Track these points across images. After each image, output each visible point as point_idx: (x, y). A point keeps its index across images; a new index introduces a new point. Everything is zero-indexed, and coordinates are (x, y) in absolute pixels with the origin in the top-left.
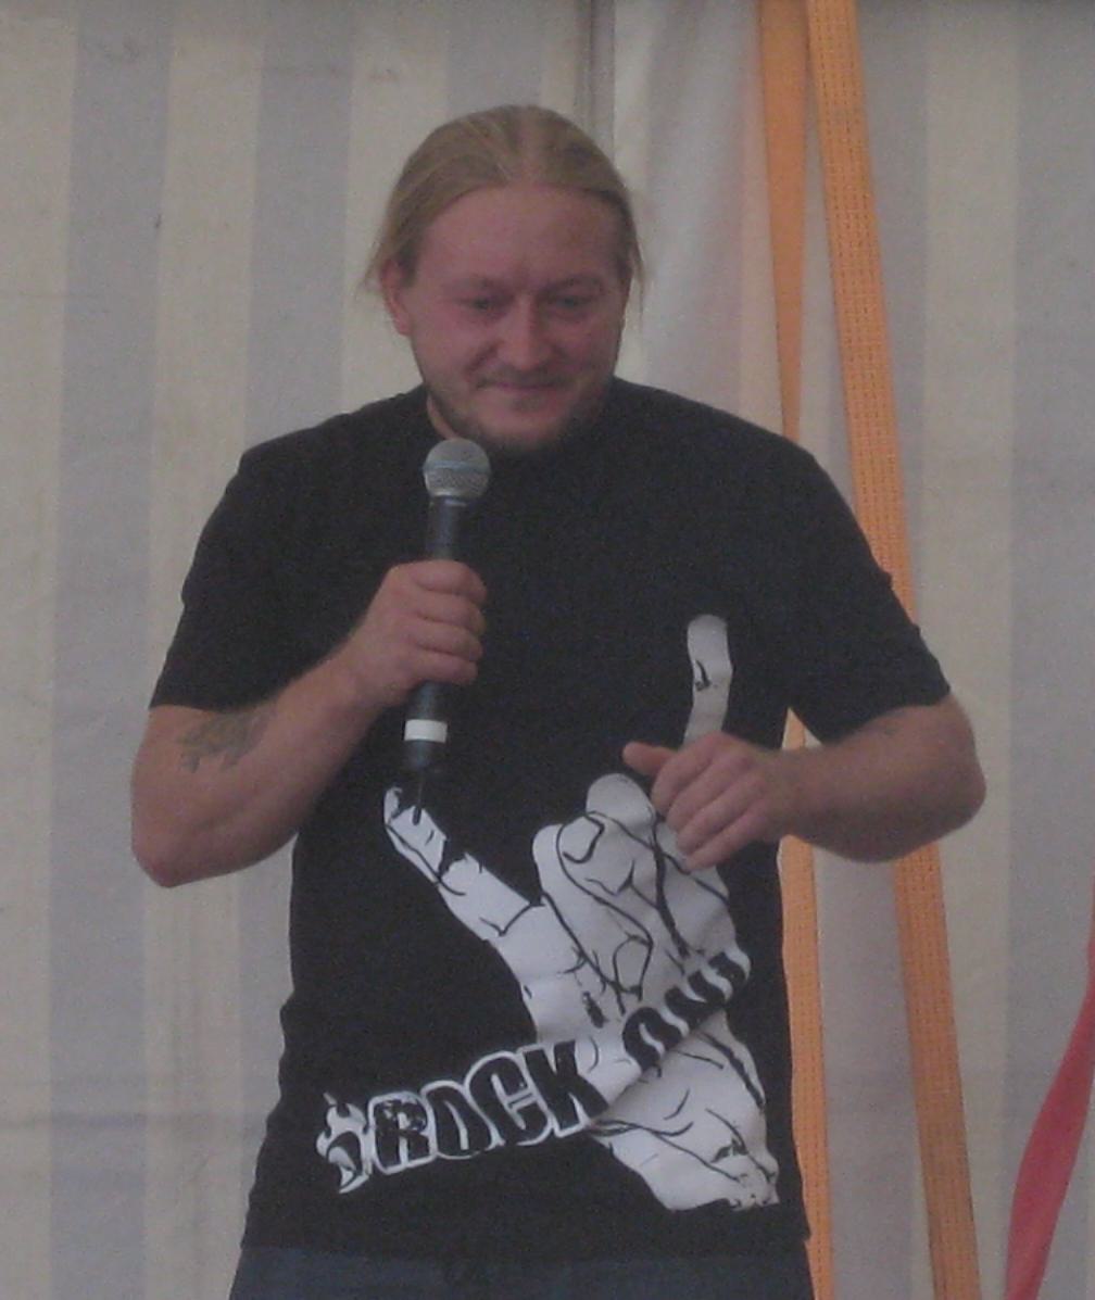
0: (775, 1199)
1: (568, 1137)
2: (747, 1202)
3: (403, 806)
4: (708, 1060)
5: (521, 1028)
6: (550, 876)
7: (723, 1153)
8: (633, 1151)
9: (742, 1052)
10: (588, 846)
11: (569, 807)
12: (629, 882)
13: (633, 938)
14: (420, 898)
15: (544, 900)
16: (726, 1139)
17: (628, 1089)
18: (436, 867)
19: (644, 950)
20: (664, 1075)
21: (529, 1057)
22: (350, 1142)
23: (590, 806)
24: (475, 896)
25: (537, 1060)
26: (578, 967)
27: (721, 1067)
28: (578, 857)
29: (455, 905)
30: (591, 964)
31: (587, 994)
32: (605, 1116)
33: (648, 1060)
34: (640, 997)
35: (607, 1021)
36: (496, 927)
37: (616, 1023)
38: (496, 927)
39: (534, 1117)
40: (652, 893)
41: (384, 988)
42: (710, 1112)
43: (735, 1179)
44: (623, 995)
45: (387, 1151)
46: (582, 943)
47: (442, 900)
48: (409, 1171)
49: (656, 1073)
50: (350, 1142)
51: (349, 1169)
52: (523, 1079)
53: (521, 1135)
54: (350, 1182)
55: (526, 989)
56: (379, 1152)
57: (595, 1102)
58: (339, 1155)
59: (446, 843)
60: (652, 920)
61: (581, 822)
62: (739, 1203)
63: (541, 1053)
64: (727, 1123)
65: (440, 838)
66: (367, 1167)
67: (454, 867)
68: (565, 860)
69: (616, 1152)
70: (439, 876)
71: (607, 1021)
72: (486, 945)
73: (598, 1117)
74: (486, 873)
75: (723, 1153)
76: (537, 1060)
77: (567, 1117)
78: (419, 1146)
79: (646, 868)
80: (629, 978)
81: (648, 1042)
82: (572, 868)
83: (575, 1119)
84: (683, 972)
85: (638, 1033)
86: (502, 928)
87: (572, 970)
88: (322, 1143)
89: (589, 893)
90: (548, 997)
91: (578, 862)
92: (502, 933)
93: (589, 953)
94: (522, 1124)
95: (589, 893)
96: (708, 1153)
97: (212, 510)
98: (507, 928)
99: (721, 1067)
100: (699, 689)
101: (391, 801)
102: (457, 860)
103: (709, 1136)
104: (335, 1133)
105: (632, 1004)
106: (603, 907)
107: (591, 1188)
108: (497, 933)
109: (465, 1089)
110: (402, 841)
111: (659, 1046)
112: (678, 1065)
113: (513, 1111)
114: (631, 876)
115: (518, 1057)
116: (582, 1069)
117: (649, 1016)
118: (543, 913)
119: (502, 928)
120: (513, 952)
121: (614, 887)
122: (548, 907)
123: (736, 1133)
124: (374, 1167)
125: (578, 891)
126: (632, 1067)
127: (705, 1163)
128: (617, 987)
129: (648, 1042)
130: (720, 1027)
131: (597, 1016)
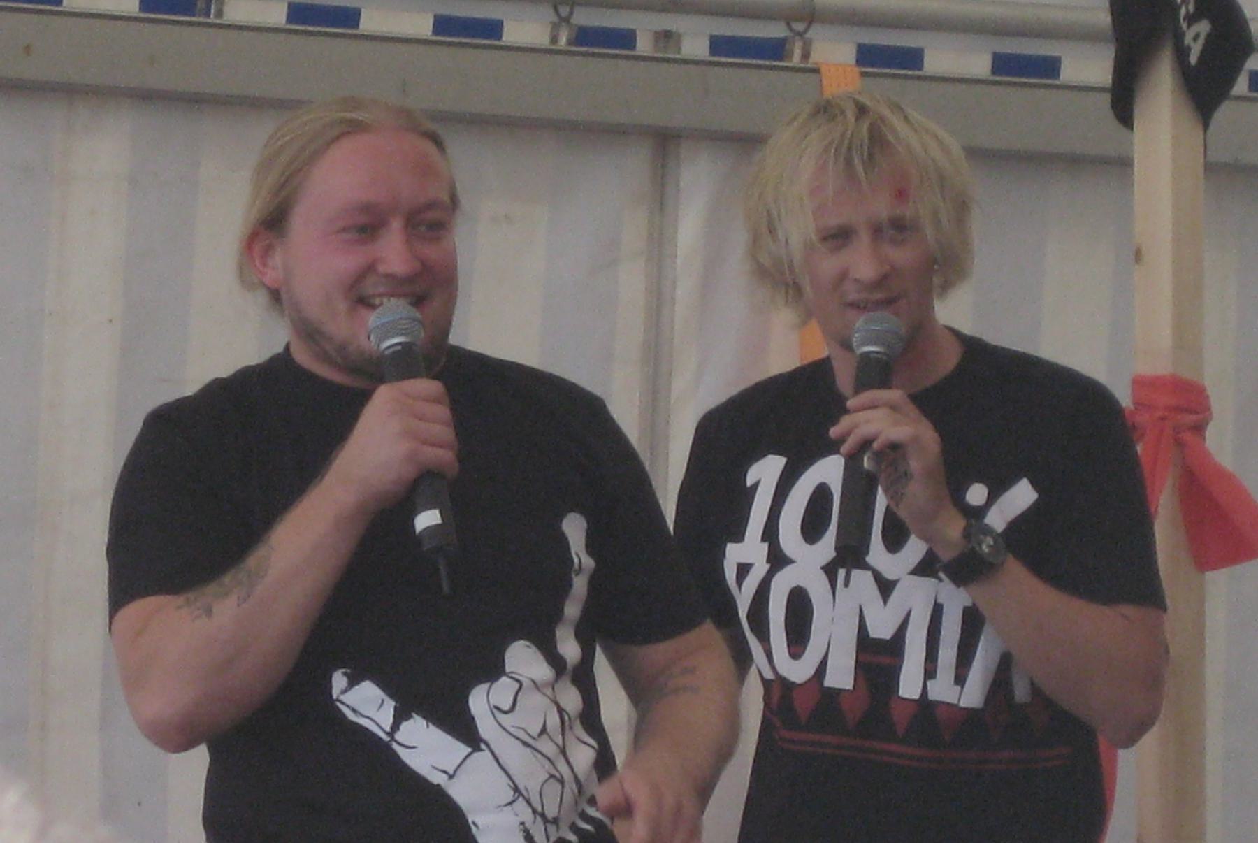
6: (485, 726)
10: (512, 699)
11: (493, 670)
12: (544, 730)
13: (552, 776)
14: (378, 755)
15: (483, 746)
18: (388, 729)
23: (508, 669)
24: (425, 748)
26: (514, 801)
31: (522, 823)
34: (558, 828)
35: (822, 568)
36: (445, 772)
38: (445, 772)
44: (549, 825)
59: (395, 708)
61: (504, 679)
65: (390, 705)
67: (405, 726)
68: (496, 712)
70: (391, 734)
71: (822, 568)
72: (438, 791)
80: (551, 812)
82: (506, 720)
86: (451, 772)
87: (510, 803)
89: (518, 739)
91: (505, 712)
93: (521, 787)
95: (518, 739)
97: (566, 377)
98: (455, 771)
102: (407, 720)
106: (528, 750)
110: (354, 711)
114: (544, 725)
118: (485, 756)
120: (459, 792)
121: (535, 734)
122: (487, 753)
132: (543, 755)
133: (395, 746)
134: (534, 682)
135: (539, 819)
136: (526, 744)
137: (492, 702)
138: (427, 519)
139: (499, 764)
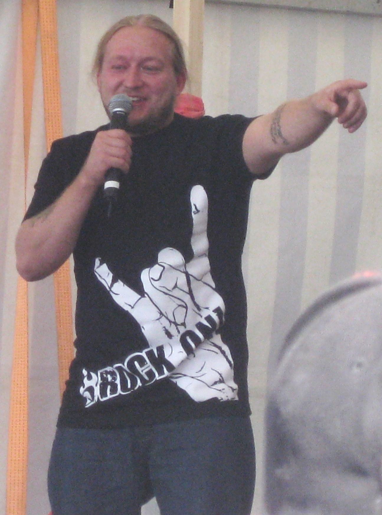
0: (237, 399)
1: (160, 379)
2: (225, 398)
3: (101, 264)
4: (213, 351)
5: (141, 342)
7: (215, 383)
8: (183, 383)
9: (225, 348)
10: (159, 275)
11: (152, 261)
12: (176, 286)
13: (180, 306)
15: (146, 295)
16: (217, 377)
17: (182, 361)
18: (109, 285)
19: (185, 310)
20: (196, 356)
21: (147, 353)
22: (91, 390)
23: (160, 260)
24: (122, 295)
25: (150, 354)
27: (217, 353)
28: (156, 279)
29: (116, 299)
30: (165, 316)
32: (174, 372)
33: (189, 350)
34: (185, 327)
36: (130, 306)
37: (177, 338)
38: (130, 306)
39: (150, 374)
40: (186, 289)
41: (105, 333)
42: (212, 369)
43: (220, 390)
45: (103, 393)
46: (161, 310)
47: (111, 297)
48: (110, 399)
49: (193, 356)
50: (91, 390)
51: (89, 399)
52: (145, 361)
53: (147, 382)
54: (89, 404)
55: (143, 327)
56: (100, 393)
57: (170, 367)
58: (87, 394)
60: (187, 298)
61: (156, 266)
62: (222, 399)
63: (152, 351)
64: (218, 372)
65: (111, 275)
66: (96, 399)
67: (116, 285)
69: (178, 384)
70: (110, 288)
72: (127, 312)
73: (172, 373)
74: (125, 286)
75: (215, 383)
76: (150, 354)
77: (161, 372)
78: (114, 390)
79: (182, 280)
80: (179, 320)
81: (190, 343)
82: (156, 284)
83: (163, 373)
84: (201, 317)
85: (186, 340)
87: (158, 319)
88: (82, 390)
90: (151, 328)
92: (132, 308)
93: (164, 312)
94: (146, 378)
96: (210, 382)
98: (134, 305)
99: (217, 353)
100: (195, 214)
101: (97, 262)
103: (211, 376)
104: (86, 386)
105: (182, 330)
106: (167, 296)
107: (165, 397)
108: (130, 307)
109: (125, 367)
110: (100, 276)
111: (193, 345)
112: (201, 353)
113: (143, 374)
114: (176, 284)
115: (143, 354)
116: (167, 356)
117: (190, 333)
119: (132, 306)
120: (135, 313)
122: (147, 298)
123: (221, 376)
124: (98, 398)
125: (158, 291)
126: (184, 354)
127: (208, 386)
128: (176, 324)
129: (190, 343)
130: (217, 339)
131: (169, 335)
132: (175, 297)
133: (111, 293)
134: (170, 266)
135: (172, 324)
136: (166, 294)
137: (151, 276)
138: (111, 184)
139: (154, 303)
